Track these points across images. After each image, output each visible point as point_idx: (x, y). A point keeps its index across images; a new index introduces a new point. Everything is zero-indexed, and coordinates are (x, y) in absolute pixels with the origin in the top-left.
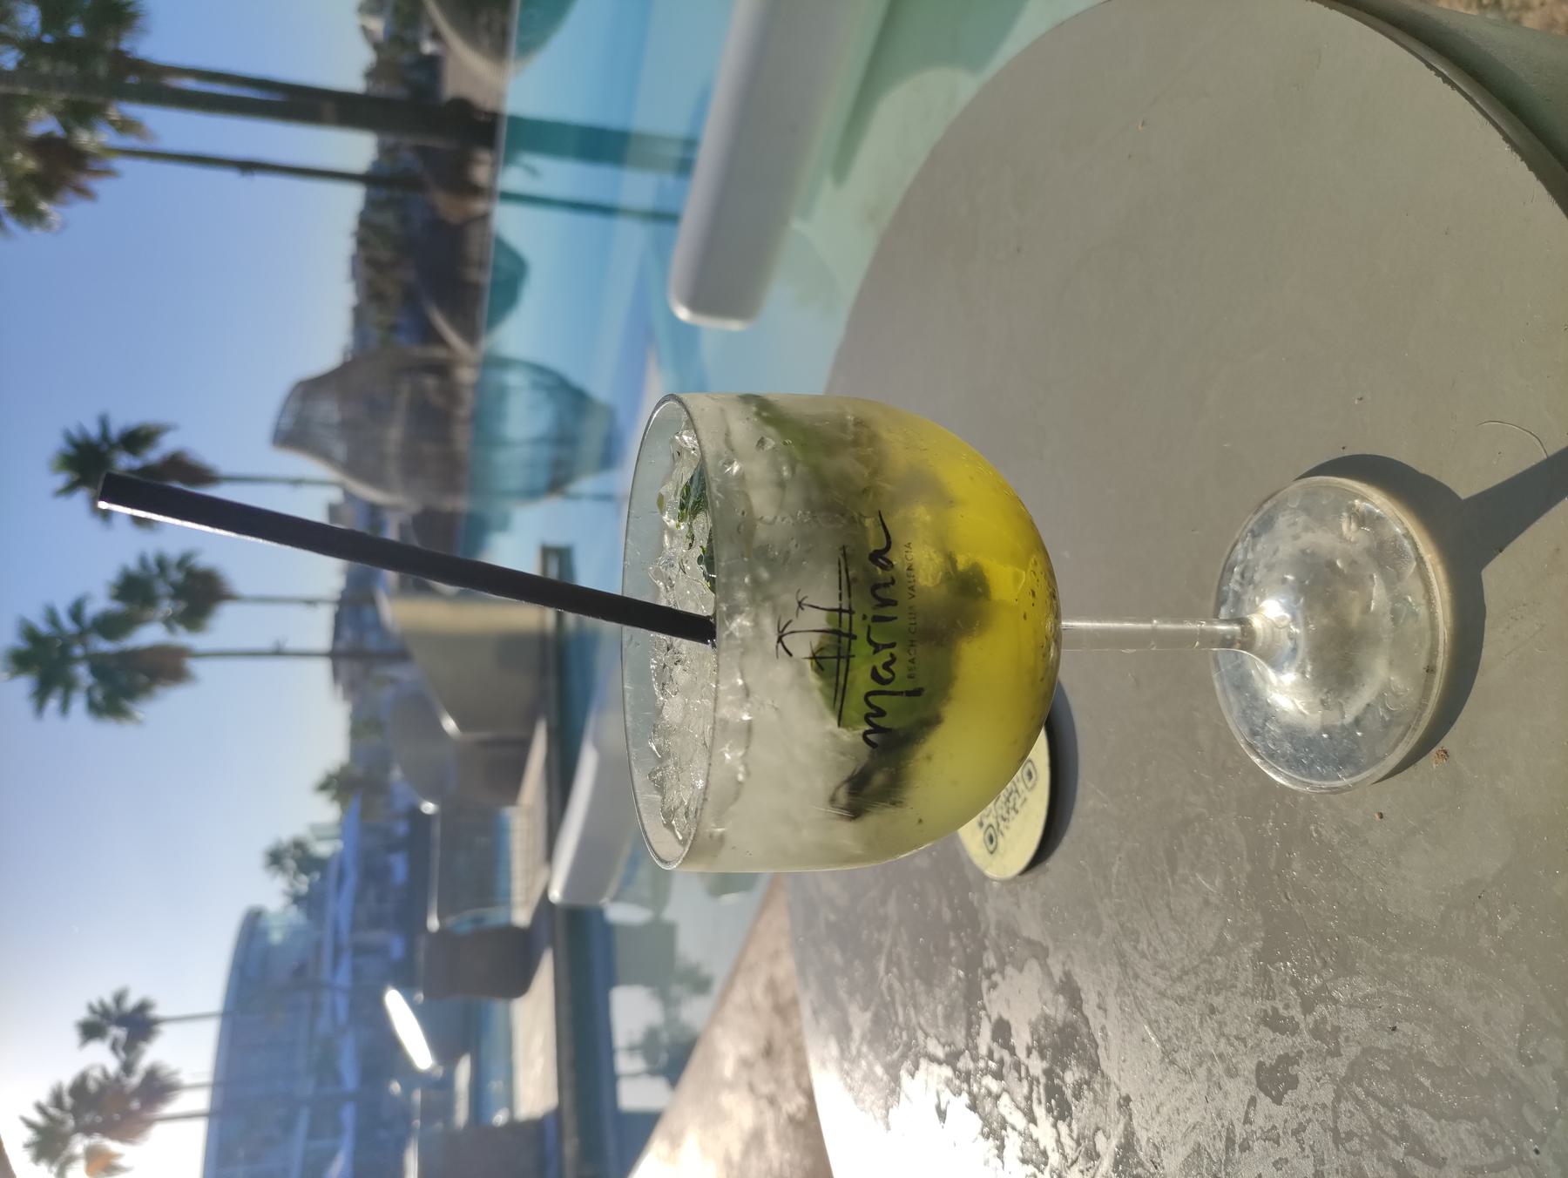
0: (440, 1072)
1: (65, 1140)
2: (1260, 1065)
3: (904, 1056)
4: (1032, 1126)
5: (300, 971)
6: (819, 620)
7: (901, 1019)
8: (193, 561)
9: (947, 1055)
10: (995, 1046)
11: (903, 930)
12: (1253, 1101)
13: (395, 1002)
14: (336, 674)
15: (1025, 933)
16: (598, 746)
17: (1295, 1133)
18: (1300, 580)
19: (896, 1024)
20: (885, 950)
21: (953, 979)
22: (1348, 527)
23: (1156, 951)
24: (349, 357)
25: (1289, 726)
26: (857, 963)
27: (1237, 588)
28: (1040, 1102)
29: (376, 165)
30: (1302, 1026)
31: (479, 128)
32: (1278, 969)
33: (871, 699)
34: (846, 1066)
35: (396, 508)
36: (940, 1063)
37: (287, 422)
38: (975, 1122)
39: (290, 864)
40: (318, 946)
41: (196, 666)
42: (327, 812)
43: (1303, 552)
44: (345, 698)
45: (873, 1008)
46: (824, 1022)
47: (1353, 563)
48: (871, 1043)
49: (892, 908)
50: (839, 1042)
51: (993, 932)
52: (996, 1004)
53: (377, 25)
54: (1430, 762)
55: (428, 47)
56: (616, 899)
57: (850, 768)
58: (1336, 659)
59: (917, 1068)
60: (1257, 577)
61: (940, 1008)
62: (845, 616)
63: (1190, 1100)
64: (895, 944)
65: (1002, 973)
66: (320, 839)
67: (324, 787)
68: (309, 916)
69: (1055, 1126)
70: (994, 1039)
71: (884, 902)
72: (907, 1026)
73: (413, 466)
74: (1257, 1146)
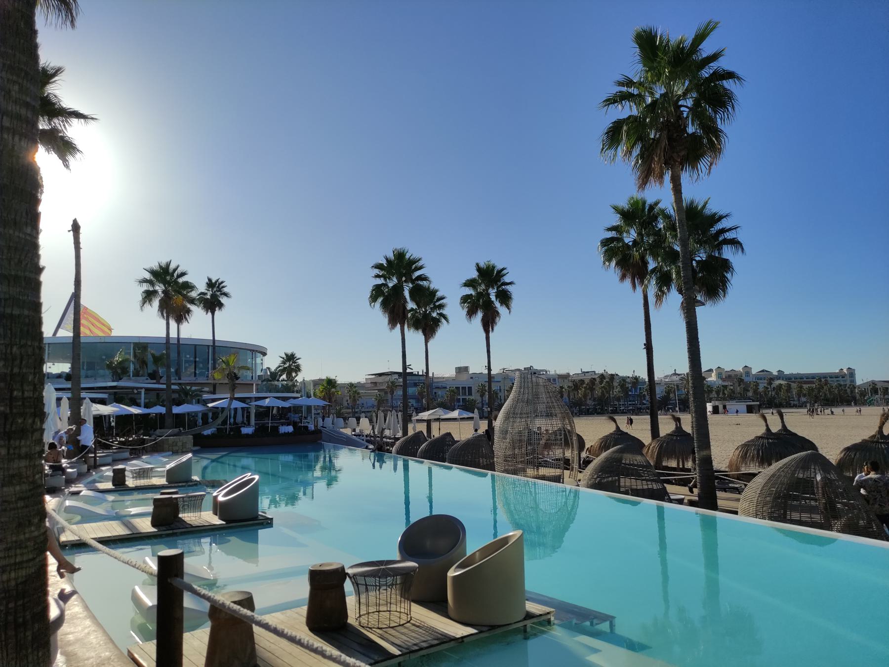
1: (164, 282)
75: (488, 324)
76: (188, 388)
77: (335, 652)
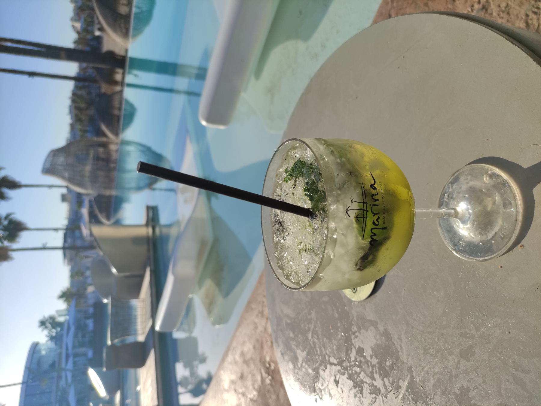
0: (108, 398)
2: (461, 350)
3: (320, 365)
4: (373, 381)
5: (53, 365)
6: (355, 206)
7: (319, 352)
8: (12, 216)
9: (338, 362)
10: (358, 357)
11: (318, 322)
12: (459, 362)
13: (92, 373)
14: (65, 255)
15: (368, 318)
16: (174, 274)
17: (475, 370)
18: (470, 196)
19: (317, 354)
20: (311, 330)
21: (340, 336)
22: (486, 179)
23: (420, 318)
24: (69, 142)
25: (468, 242)
26: (300, 336)
27: (446, 200)
28: (376, 373)
29: (78, 73)
30: (476, 335)
31: (119, 61)
32: (466, 319)
33: (373, 230)
34: (296, 371)
35: (88, 195)
36: (335, 365)
37: (48, 165)
38: (350, 383)
39: (49, 326)
40: (60, 354)
41: (13, 254)
42: (62, 305)
43: (471, 187)
44: (68, 264)
45: (307, 350)
46: (286, 358)
47: (488, 190)
48: (306, 363)
49: (313, 315)
50: (293, 363)
51: (355, 319)
52: (357, 343)
53: (78, 25)
54: (518, 248)
55: (97, 33)
56: (178, 330)
57: (362, 254)
58: (484, 221)
59: (326, 368)
60: (454, 196)
61: (335, 346)
62: (365, 204)
63: (435, 364)
64: (315, 327)
65: (360, 332)
66: (60, 316)
67: (61, 297)
68: (56, 344)
69: (383, 380)
70: (357, 354)
71: (310, 314)
72: (321, 354)
73: (94, 179)
74: (461, 376)
75: (14, 185)
76: (59, 393)
77: (489, 257)
